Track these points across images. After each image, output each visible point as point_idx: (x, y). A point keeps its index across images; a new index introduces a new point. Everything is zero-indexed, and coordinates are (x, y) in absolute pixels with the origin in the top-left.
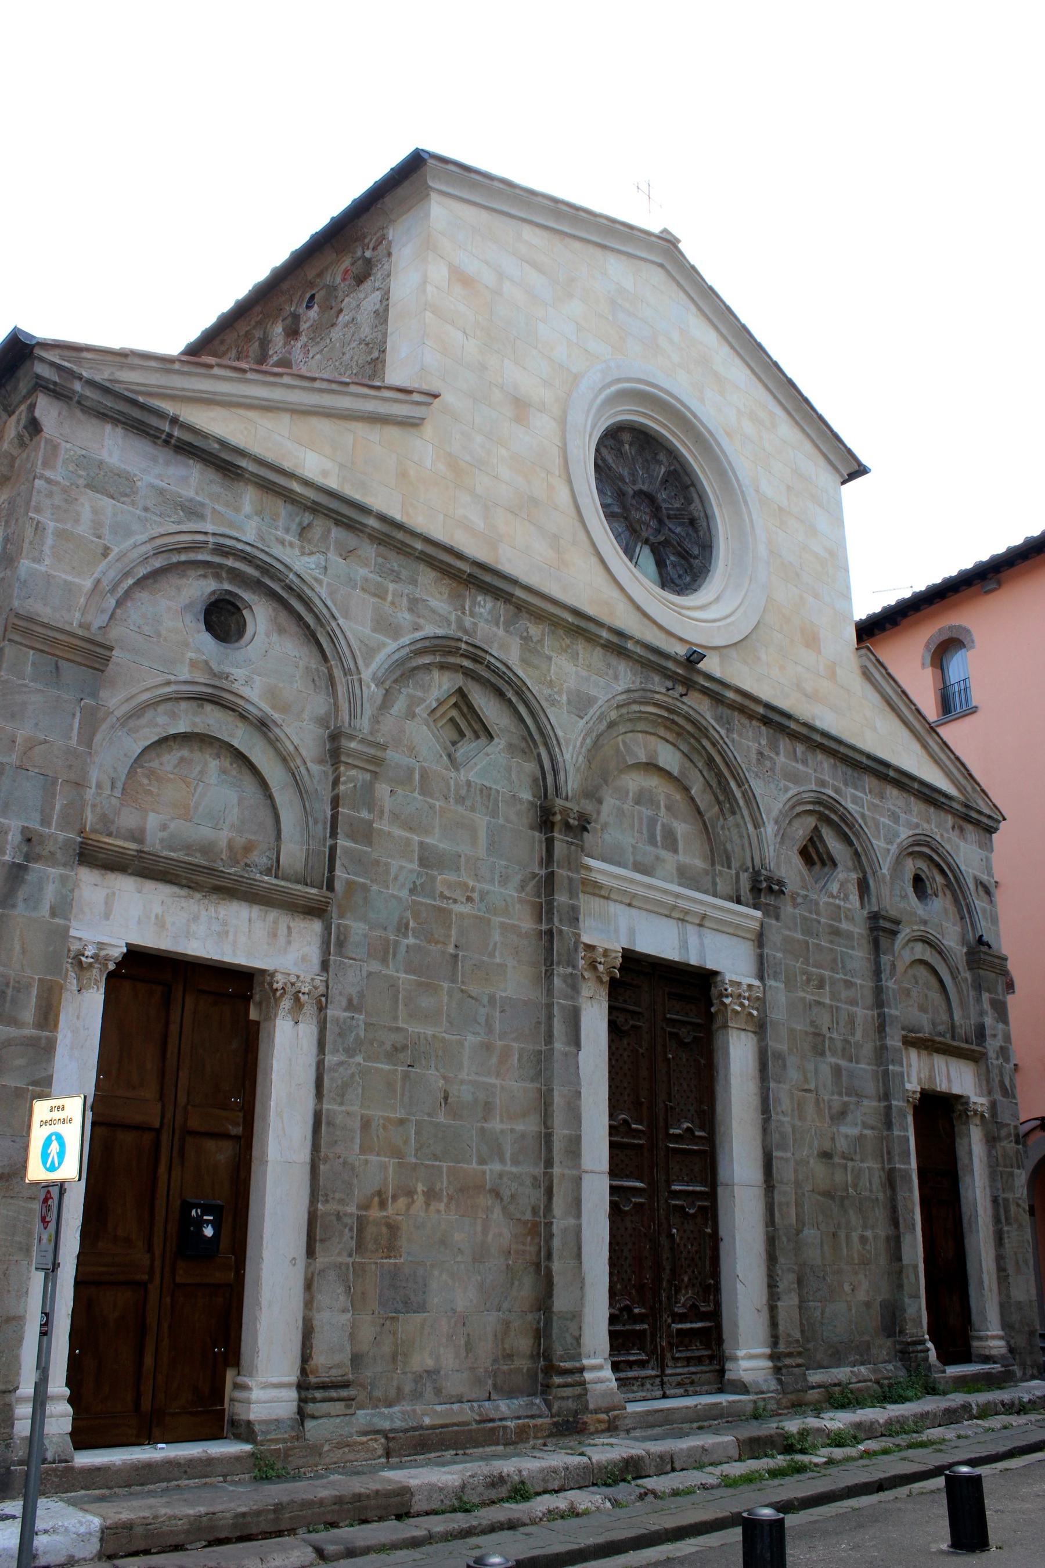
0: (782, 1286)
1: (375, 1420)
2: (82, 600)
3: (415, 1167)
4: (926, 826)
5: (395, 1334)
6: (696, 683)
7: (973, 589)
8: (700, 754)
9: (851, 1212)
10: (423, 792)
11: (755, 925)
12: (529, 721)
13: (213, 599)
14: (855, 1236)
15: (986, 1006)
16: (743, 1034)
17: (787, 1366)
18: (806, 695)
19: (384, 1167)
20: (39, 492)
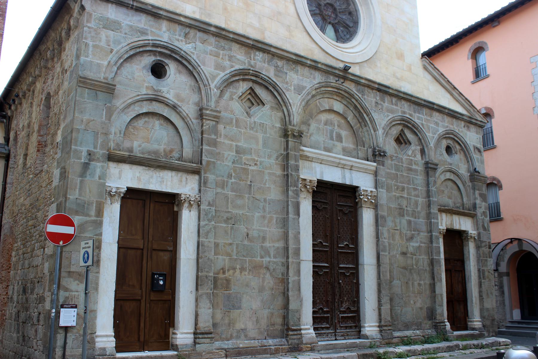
0: (383, 301)
1: (222, 345)
2: (104, 69)
3: (236, 260)
4: (451, 126)
5: (229, 316)
6: (348, 78)
7: (488, 26)
8: (352, 105)
9: (414, 275)
10: (237, 127)
11: (374, 168)
12: (279, 98)
13: (154, 63)
14: (416, 283)
15: (477, 195)
16: (369, 209)
17: (384, 330)
18: (397, 78)
19: (224, 260)
20: (86, 32)
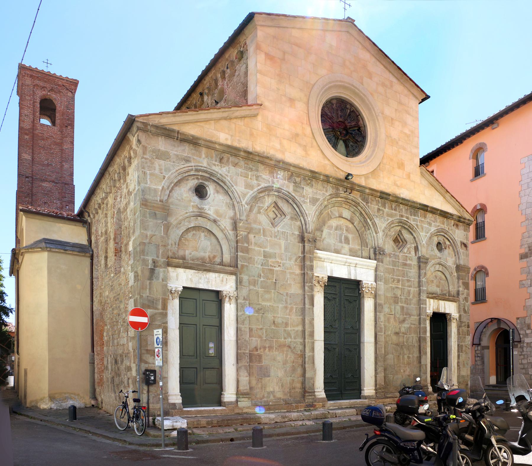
4: (442, 226)
10: (264, 236)
12: (297, 209)
14: (406, 357)
15: (461, 284)
